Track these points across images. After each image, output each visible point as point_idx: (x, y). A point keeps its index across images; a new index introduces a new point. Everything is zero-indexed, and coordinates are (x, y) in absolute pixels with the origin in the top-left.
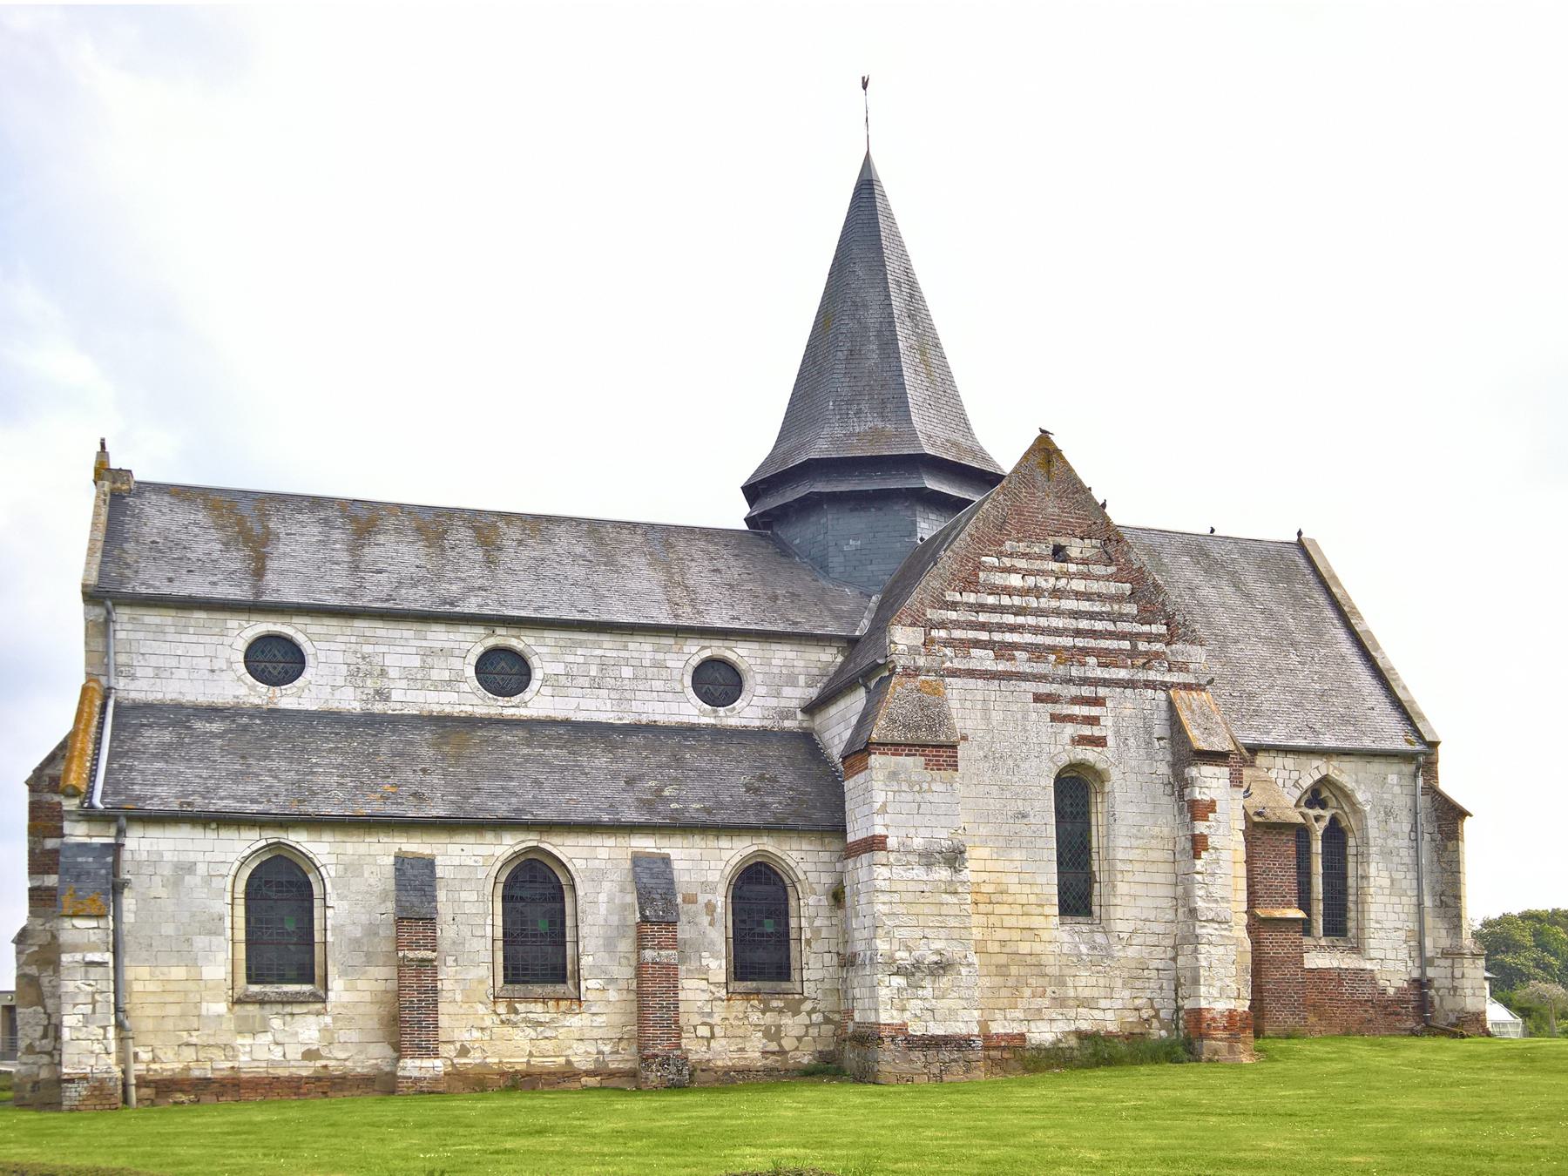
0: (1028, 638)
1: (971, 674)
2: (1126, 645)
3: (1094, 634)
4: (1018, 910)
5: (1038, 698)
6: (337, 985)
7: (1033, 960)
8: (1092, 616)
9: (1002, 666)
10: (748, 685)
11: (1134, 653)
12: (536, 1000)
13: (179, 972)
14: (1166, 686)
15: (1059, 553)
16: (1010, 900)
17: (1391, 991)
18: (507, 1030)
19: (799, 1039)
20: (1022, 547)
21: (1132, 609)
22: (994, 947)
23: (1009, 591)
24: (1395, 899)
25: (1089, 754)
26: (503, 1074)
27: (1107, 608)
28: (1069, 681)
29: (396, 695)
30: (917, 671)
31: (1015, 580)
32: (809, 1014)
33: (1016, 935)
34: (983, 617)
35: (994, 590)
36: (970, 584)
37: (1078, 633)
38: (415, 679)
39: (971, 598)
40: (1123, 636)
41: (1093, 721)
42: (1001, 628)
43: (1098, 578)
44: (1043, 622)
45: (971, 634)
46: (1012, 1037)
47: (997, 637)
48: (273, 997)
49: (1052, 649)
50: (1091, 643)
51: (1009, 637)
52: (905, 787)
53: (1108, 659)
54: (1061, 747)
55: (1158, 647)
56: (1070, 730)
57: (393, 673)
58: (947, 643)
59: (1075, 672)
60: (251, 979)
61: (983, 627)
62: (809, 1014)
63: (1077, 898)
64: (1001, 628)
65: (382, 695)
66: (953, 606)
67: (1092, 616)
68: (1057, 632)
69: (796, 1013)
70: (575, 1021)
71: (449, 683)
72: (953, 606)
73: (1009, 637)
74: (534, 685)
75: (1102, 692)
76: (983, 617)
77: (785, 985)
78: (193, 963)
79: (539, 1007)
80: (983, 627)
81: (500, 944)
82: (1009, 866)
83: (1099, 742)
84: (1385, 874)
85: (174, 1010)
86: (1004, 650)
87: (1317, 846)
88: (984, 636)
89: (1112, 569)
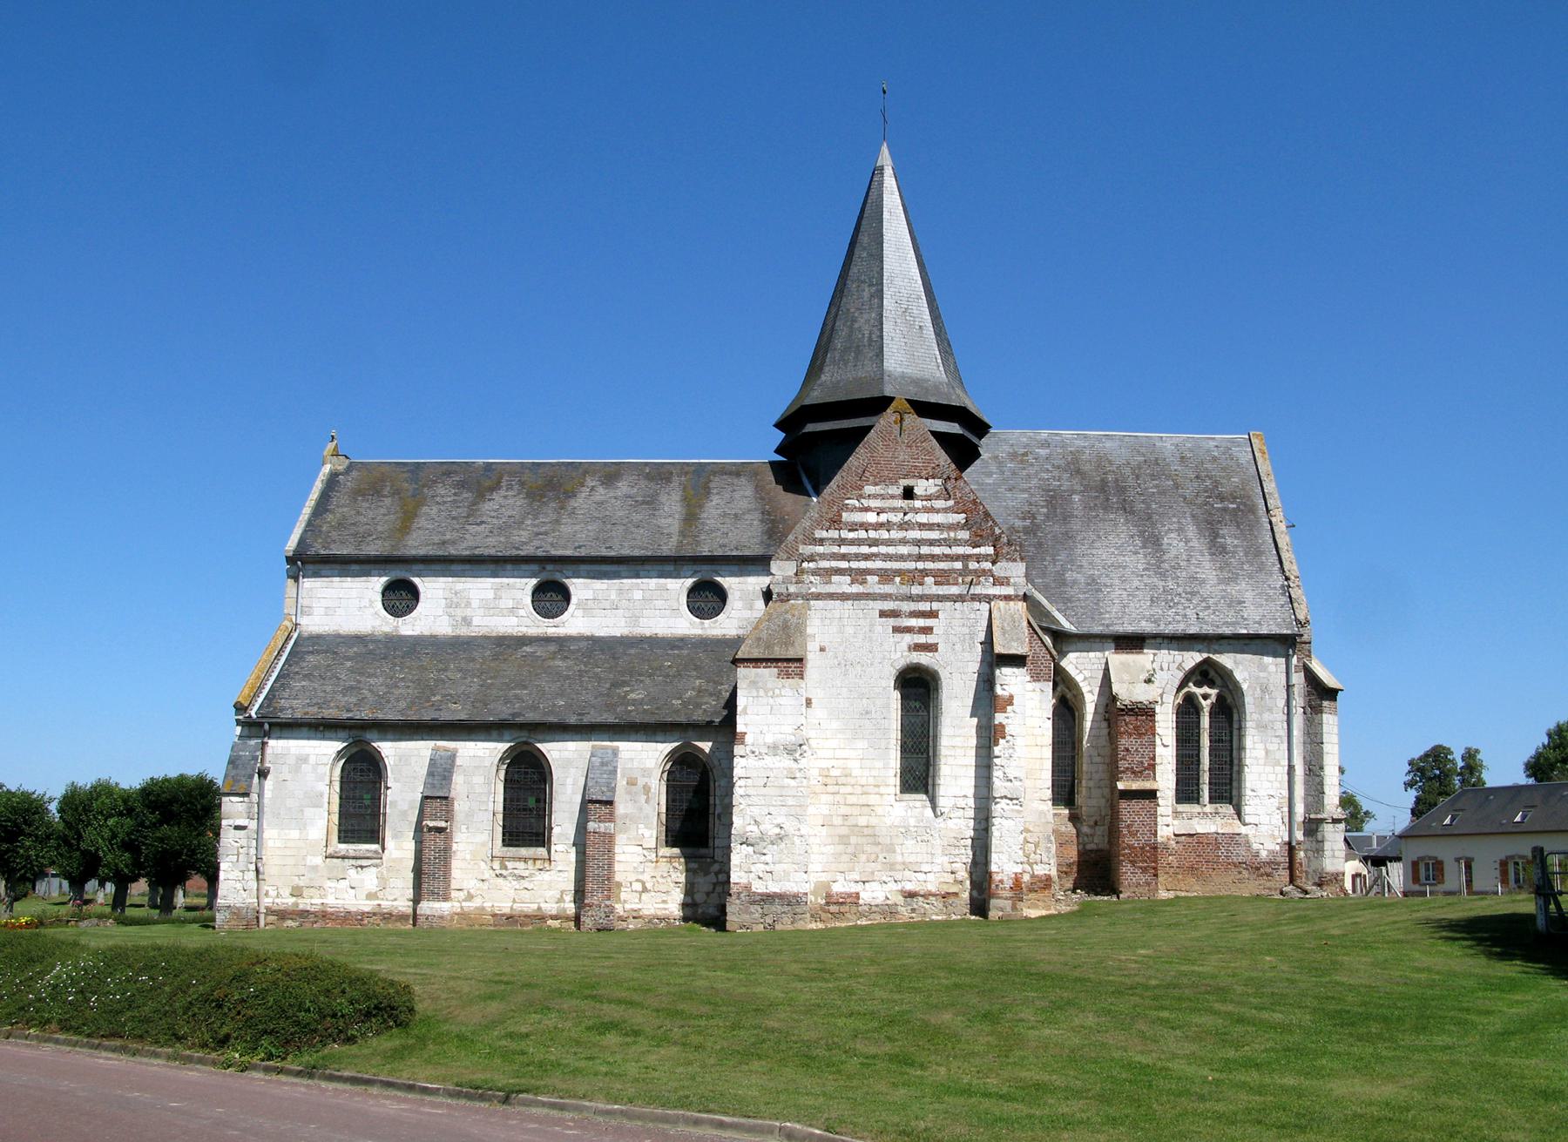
0: (879, 564)
1: (831, 596)
2: (958, 565)
3: (933, 558)
4: (859, 790)
5: (883, 614)
6: (389, 843)
7: (866, 831)
8: (932, 543)
9: (856, 589)
10: (730, 598)
11: (965, 571)
12: (520, 859)
13: (295, 834)
14: (989, 599)
15: (908, 493)
16: (853, 781)
17: (1264, 854)
18: (500, 880)
19: (708, 894)
20: (877, 490)
21: (964, 535)
22: (838, 821)
23: (865, 527)
24: (1269, 769)
25: (924, 659)
26: (494, 915)
27: (945, 535)
28: (910, 598)
29: (476, 621)
30: (789, 597)
31: (871, 518)
32: (716, 874)
33: (856, 811)
34: (844, 550)
35: (853, 527)
36: (836, 522)
37: (920, 558)
38: (490, 608)
39: (834, 534)
40: (957, 558)
41: (927, 630)
42: (858, 557)
43: (938, 511)
44: (891, 550)
45: (834, 564)
46: (850, 895)
47: (854, 565)
48: (352, 853)
49: (899, 572)
50: (930, 565)
51: (863, 565)
52: (762, 693)
53: (942, 577)
54: (899, 653)
55: (987, 565)
56: (908, 639)
57: (475, 604)
58: (815, 572)
59: (916, 590)
60: (341, 840)
61: (844, 557)
62: (716, 874)
63: (918, 773)
64: (858, 557)
65: (467, 621)
66: (821, 541)
67: (932, 543)
68: (902, 558)
69: (707, 873)
70: (546, 876)
71: (513, 611)
72: (821, 541)
73: (863, 565)
74: (572, 607)
75: (935, 605)
76: (844, 550)
77: (703, 851)
78: (303, 826)
79: (521, 865)
80: (844, 557)
81: (500, 817)
82: (853, 754)
83: (931, 648)
84: (1261, 746)
85: (291, 861)
86: (859, 576)
87: (1205, 721)
88: (844, 565)
89: (951, 503)
